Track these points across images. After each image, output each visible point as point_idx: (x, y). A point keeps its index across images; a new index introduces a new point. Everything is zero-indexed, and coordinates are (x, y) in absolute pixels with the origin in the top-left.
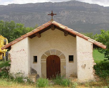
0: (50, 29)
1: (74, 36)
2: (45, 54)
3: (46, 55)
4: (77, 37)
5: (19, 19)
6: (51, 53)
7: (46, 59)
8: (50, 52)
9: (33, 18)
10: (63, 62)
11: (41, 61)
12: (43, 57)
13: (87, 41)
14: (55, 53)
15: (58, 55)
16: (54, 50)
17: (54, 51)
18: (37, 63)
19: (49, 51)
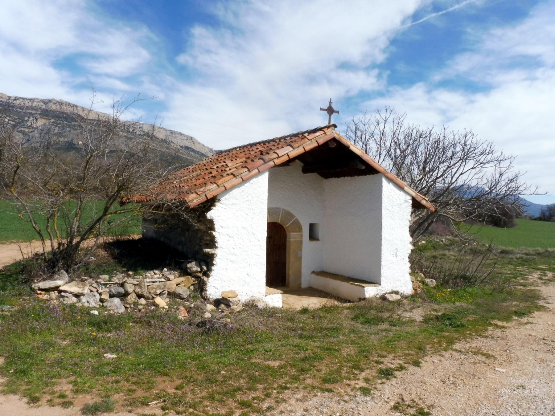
13: (402, 193)
14: (278, 218)
16: (277, 208)
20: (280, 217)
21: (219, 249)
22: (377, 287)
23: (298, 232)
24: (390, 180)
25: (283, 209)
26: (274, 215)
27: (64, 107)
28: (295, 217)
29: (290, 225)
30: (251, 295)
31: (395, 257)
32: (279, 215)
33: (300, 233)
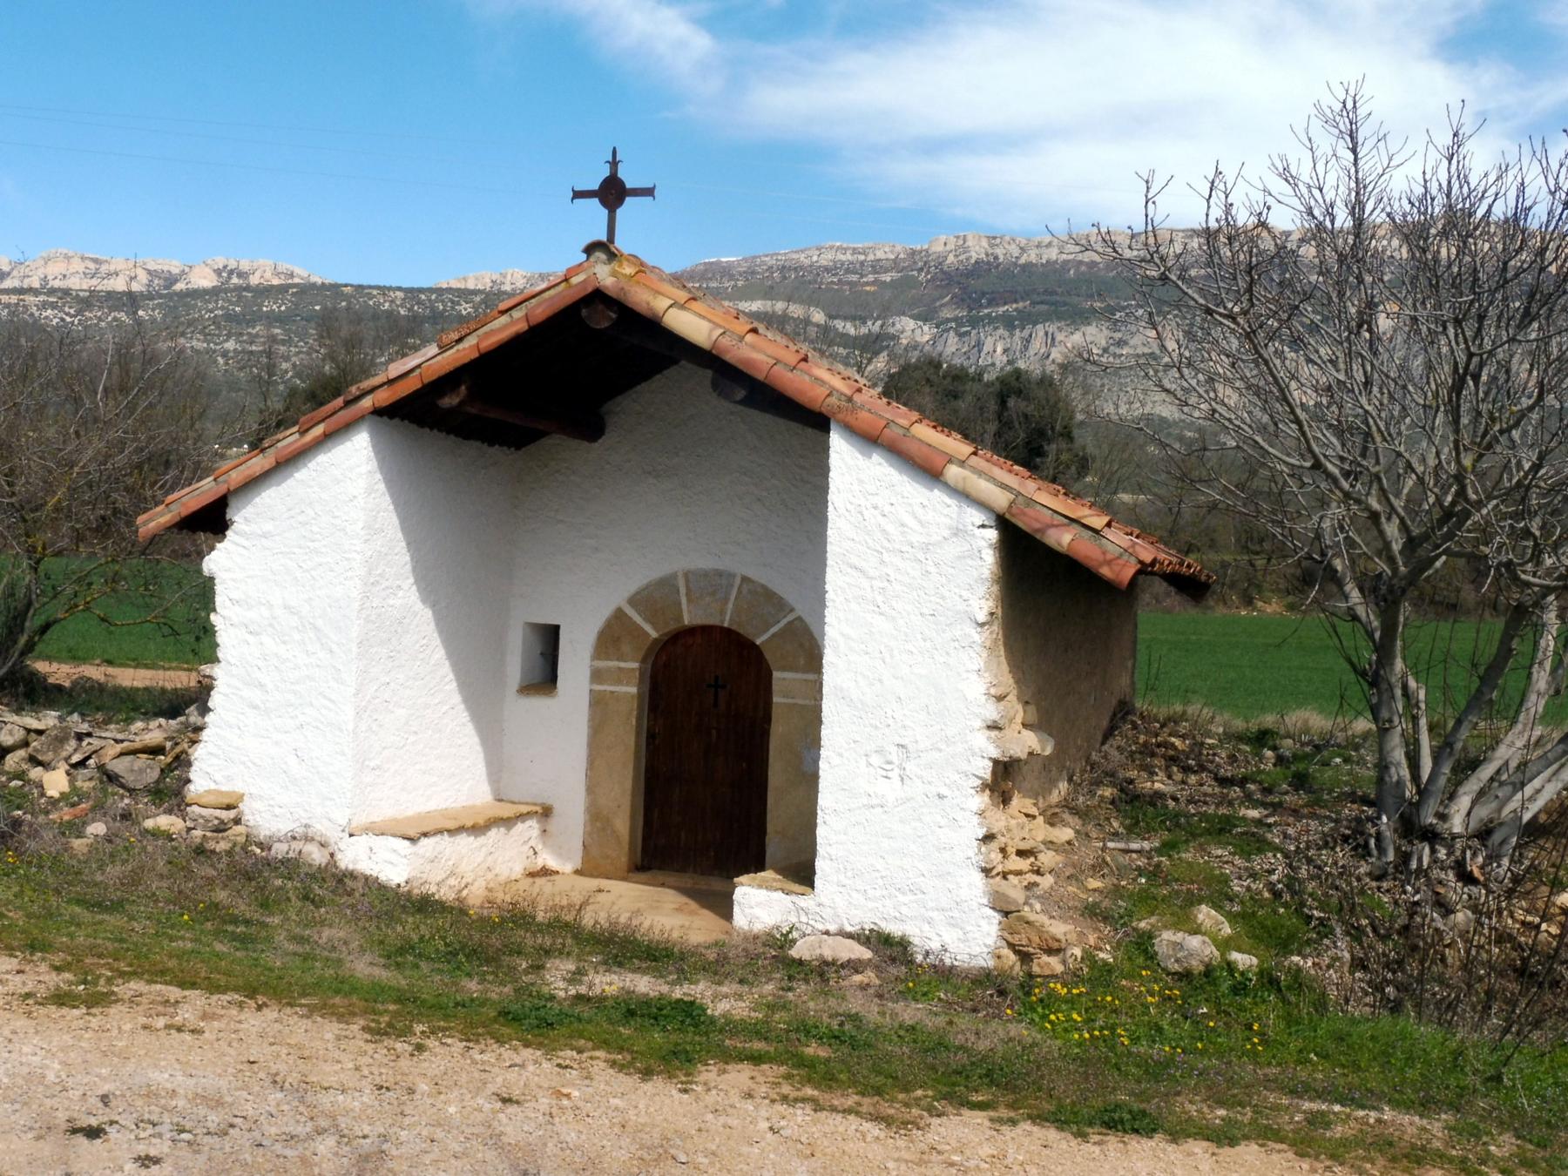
0: (709, 373)
1: (819, 422)
2: (631, 612)
3: (638, 619)
4: (840, 447)
5: (1005, 351)
6: (684, 600)
7: (635, 665)
8: (683, 591)
9: (1118, 351)
10: (800, 702)
11: (597, 676)
12: (612, 637)
13: (938, 496)
14: (722, 613)
15: (746, 631)
16: (719, 574)
17: (711, 583)
18: (553, 697)
19: (667, 583)
20: (730, 605)
21: (223, 664)
22: (794, 898)
24: (870, 439)
25: (745, 579)
27: (575, 280)
30: (304, 822)
31: (896, 779)
32: (726, 600)
33: (811, 677)
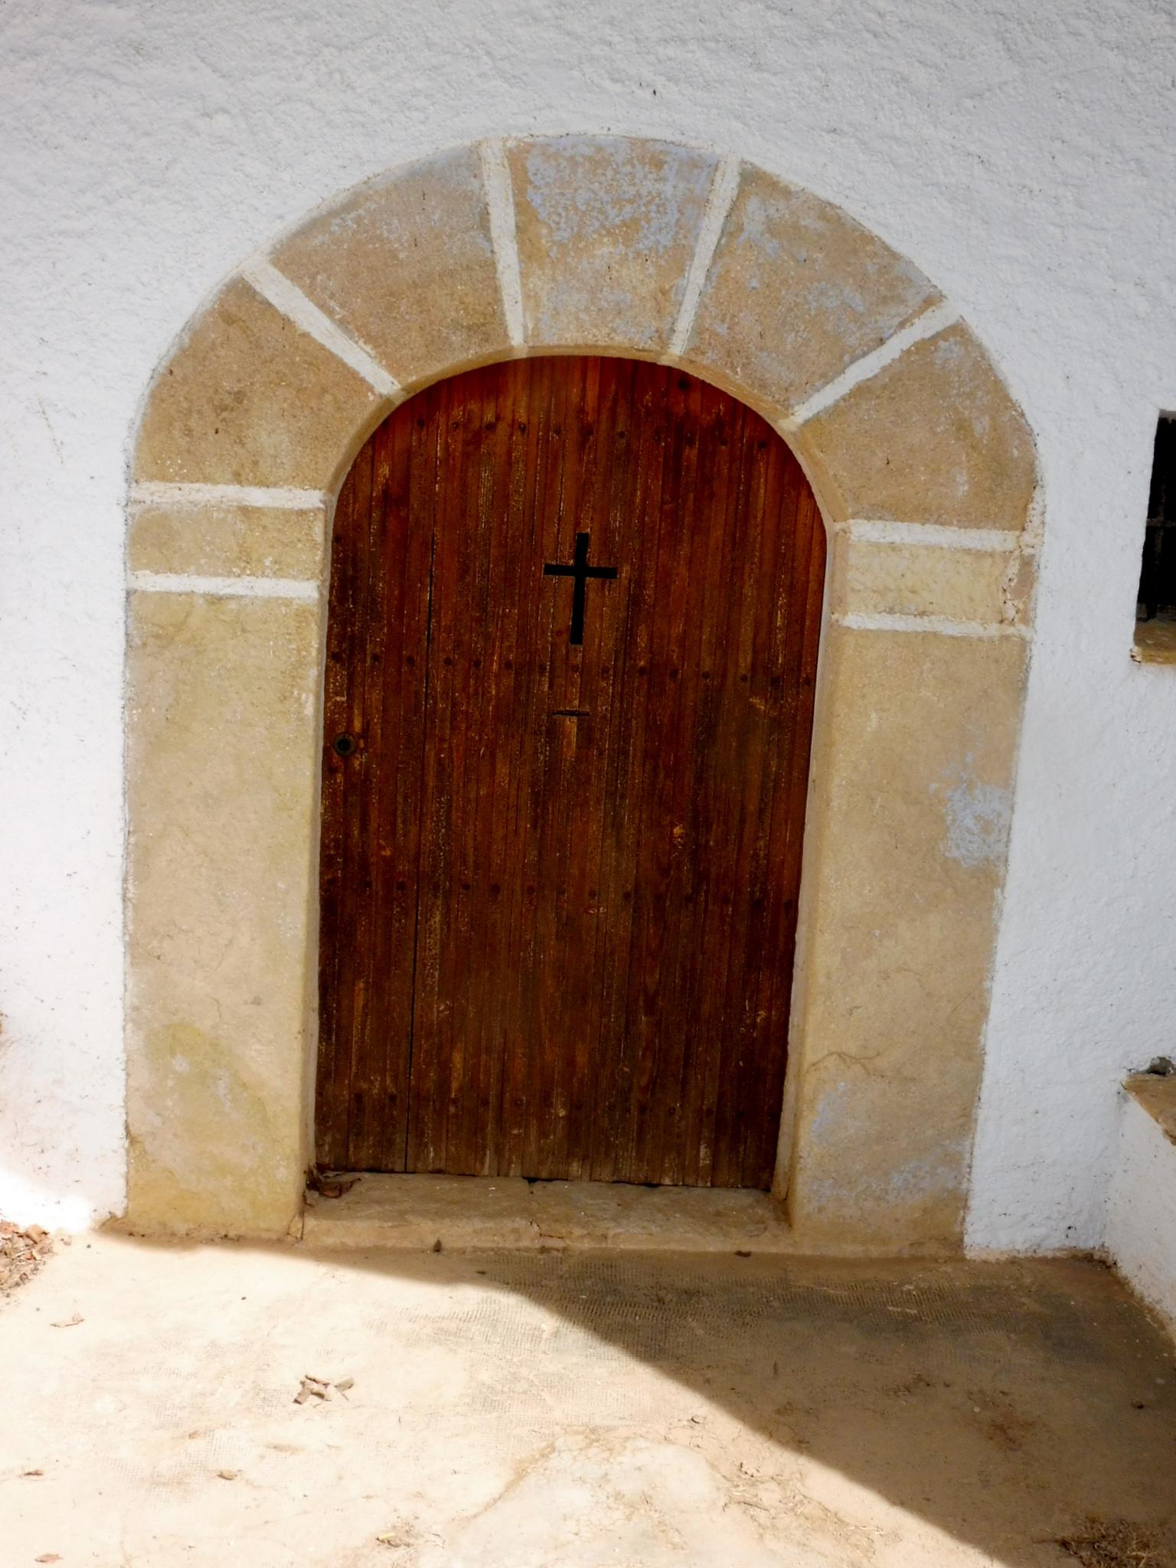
14: (664, 300)
20: (696, 277)
23: (971, 517)
25: (752, 179)
26: (605, 250)
28: (470, 161)
29: (836, 411)
32: (679, 257)
33: (993, 539)
